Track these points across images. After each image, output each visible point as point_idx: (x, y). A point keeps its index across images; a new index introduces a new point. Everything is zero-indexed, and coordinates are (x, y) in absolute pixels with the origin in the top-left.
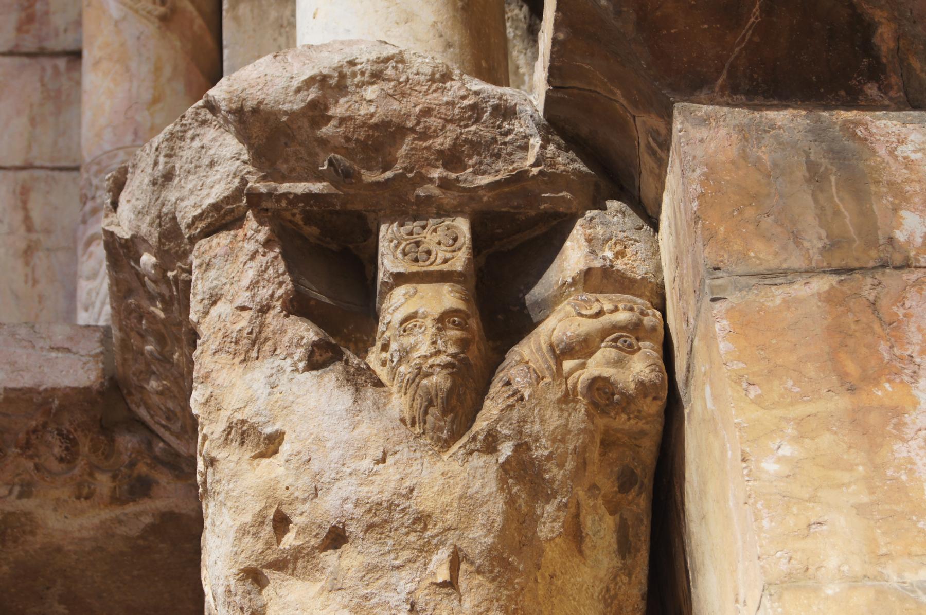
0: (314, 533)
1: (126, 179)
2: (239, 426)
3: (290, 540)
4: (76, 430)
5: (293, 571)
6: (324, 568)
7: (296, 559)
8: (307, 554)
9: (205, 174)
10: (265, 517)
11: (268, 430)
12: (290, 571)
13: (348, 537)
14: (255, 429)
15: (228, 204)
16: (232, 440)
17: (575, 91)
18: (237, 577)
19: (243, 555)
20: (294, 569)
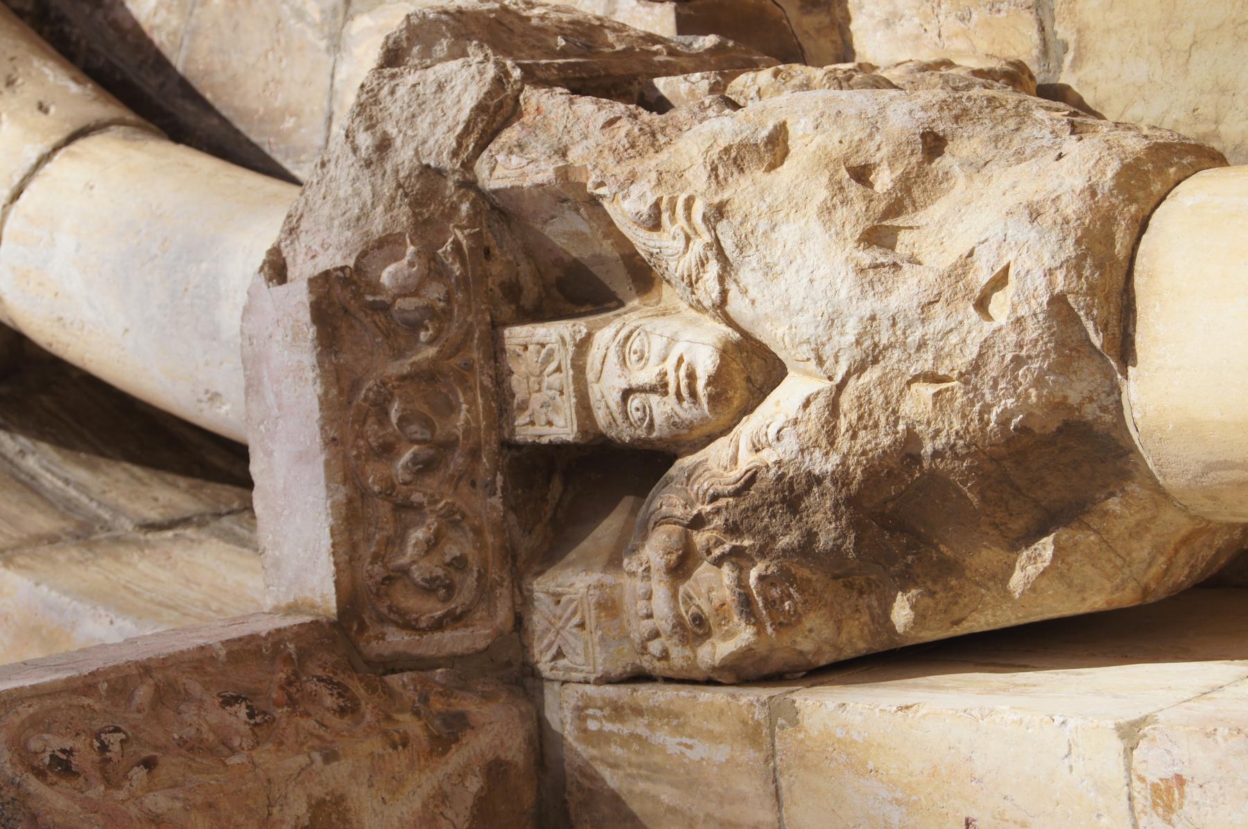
0: (909, 152)
1: (284, 259)
2: (725, 158)
3: (884, 180)
4: (335, 674)
5: (914, 205)
6: (947, 173)
7: (908, 190)
8: (918, 176)
9: (437, 102)
10: (840, 182)
11: (764, 133)
12: (910, 210)
13: (944, 136)
14: (745, 146)
15: (492, 100)
16: (726, 179)
18: (861, 248)
19: (847, 227)
20: (914, 203)
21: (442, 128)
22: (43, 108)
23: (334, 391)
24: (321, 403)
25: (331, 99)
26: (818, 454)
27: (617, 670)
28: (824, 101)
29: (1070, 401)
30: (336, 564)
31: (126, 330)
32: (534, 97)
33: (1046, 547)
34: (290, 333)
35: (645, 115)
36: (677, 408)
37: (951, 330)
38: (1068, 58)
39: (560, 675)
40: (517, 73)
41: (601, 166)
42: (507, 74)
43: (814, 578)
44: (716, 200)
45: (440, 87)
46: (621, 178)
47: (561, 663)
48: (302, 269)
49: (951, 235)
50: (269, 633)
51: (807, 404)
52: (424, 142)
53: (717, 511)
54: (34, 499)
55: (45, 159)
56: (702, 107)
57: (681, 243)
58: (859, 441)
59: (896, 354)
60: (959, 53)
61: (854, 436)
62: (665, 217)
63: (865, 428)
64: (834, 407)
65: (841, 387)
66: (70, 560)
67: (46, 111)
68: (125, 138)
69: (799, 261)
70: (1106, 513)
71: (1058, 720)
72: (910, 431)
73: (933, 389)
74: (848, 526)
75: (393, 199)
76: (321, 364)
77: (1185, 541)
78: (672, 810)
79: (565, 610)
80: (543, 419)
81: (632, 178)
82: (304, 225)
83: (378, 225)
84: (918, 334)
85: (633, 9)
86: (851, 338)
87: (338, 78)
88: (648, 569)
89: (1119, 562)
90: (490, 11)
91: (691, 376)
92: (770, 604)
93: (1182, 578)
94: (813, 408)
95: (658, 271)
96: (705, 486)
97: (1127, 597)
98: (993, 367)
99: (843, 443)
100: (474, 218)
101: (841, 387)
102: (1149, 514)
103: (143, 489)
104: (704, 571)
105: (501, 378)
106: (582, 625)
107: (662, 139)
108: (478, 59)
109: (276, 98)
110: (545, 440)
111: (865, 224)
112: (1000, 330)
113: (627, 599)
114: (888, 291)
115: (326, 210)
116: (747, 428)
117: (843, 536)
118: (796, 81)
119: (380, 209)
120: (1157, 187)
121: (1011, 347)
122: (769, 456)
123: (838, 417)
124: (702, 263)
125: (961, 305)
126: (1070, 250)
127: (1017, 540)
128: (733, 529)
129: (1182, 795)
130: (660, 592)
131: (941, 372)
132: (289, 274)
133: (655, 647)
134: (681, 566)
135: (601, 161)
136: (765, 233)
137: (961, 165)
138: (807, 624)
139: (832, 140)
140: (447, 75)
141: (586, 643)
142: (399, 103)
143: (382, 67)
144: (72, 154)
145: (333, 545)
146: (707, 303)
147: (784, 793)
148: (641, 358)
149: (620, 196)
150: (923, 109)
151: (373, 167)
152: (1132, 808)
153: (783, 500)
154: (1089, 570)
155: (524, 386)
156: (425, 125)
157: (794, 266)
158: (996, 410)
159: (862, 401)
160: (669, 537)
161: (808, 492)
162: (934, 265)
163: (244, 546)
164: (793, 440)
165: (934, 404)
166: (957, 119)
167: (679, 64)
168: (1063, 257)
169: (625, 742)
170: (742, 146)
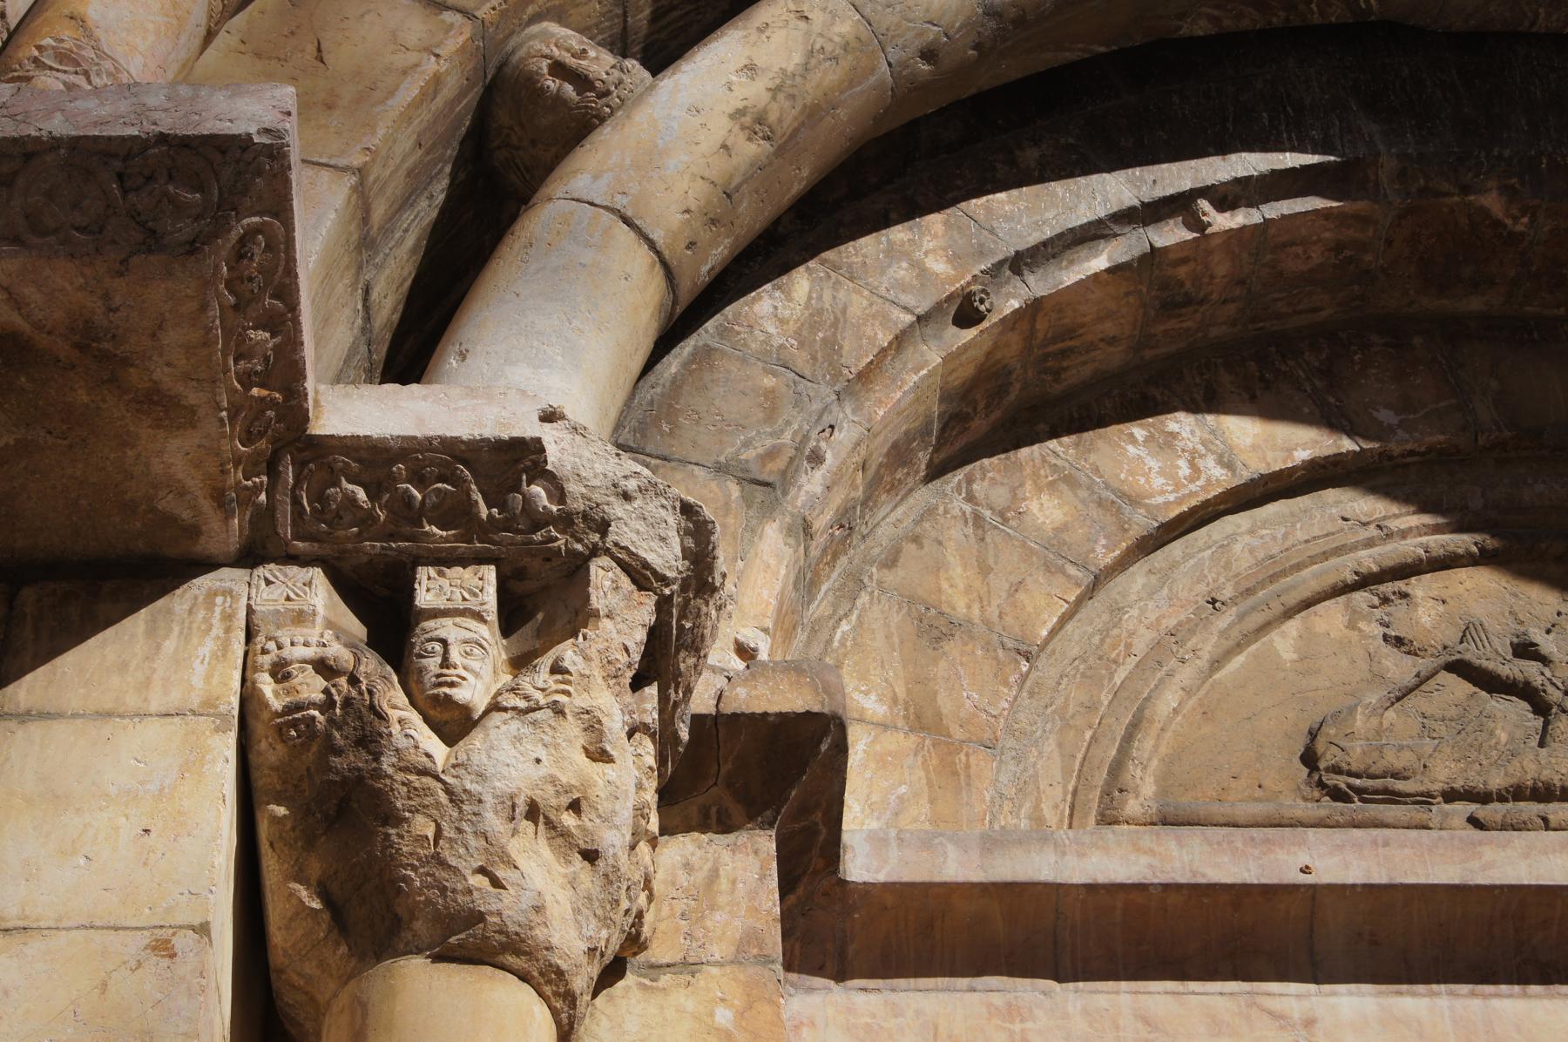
3: (569, 820)
11: (608, 748)
16: (580, 719)
17: (714, 733)
21: (634, 537)
22: (691, 245)
23: (463, 447)
24: (456, 438)
25: (679, 461)
26: (394, 760)
27: (256, 619)
28: (626, 790)
29: (415, 922)
30: (345, 437)
31: (518, 295)
32: (650, 601)
33: (316, 904)
34: (505, 422)
35: (630, 674)
36: (431, 674)
37: (467, 849)
38: (647, 982)
39: (255, 581)
40: (667, 591)
41: (597, 639)
42: (667, 585)
43: (310, 755)
44: (567, 711)
45: (663, 539)
46: (588, 651)
47: (263, 583)
48: (551, 437)
49: (530, 858)
50: (305, 389)
51: (428, 755)
52: (626, 524)
53: (361, 693)
54: (396, 206)
55: (652, 245)
56: (631, 713)
57: (541, 684)
58: (400, 787)
59: (455, 814)
60: (659, 910)
61: (403, 784)
62: (559, 677)
63: (409, 791)
64: (423, 772)
65: (437, 778)
66: (351, 234)
67: (688, 248)
68: (662, 305)
69: (522, 759)
70: (338, 944)
71: (214, 889)
72: (406, 820)
73: (431, 835)
74: (344, 777)
75: (589, 500)
76: (483, 440)
77: (313, 1000)
78: (158, 647)
79: (299, 588)
80: (431, 586)
81: (587, 658)
82: (578, 438)
83: (572, 487)
84: (467, 829)
85: (715, 686)
86: (468, 786)
87: (696, 468)
88: (324, 645)
89: (304, 953)
90: (713, 578)
91: (452, 685)
92: (294, 724)
93: (286, 999)
94: (425, 759)
95: (523, 671)
96: (379, 687)
97: (277, 958)
98: (441, 874)
99: (400, 777)
100: (572, 553)
101: (437, 778)
102: (334, 972)
103: (394, 286)
104: (320, 682)
105: (464, 562)
106: (288, 599)
107: (612, 682)
108: (680, 567)
109: (686, 419)
110: (417, 586)
111: (541, 804)
112: (466, 880)
113: (305, 630)
114: (496, 812)
115: (587, 454)
116: (414, 717)
117: (337, 773)
118: (644, 781)
119: (584, 490)
120: (548, 990)
121: (453, 886)
122: (395, 729)
123: (418, 775)
124: (527, 698)
125: (483, 857)
126: (512, 928)
127: (325, 887)
128: (348, 702)
129: (163, 956)
130: (310, 653)
131: (441, 842)
132: (546, 424)
133: (271, 645)
134: (323, 667)
135: (601, 640)
136: (542, 739)
137: (575, 873)
138: (280, 747)
139: (599, 790)
140: (670, 544)
141: (276, 601)
142: (654, 510)
143: (681, 501)
144: (653, 265)
145: (358, 436)
146: (500, 699)
147: (168, 720)
148: (466, 653)
149: (576, 649)
150: (615, 855)
151: (613, 488)
152: (155, 927)
153: (365, 736)
154: (300, 932)
155: (455, 575)
156: (638, 527)
157: (518, 756)
158: (412, 874)
159: (427, 791)
160: (346, 661)
161: (369, 752)
162: (510, 845)
163: (345, 362)
164: (405, 745)
165: (420, 836)
166: (606, 875)
167: (667, 709)
168: (508, 923)
169: (206, 620)
170: (601, 732)
